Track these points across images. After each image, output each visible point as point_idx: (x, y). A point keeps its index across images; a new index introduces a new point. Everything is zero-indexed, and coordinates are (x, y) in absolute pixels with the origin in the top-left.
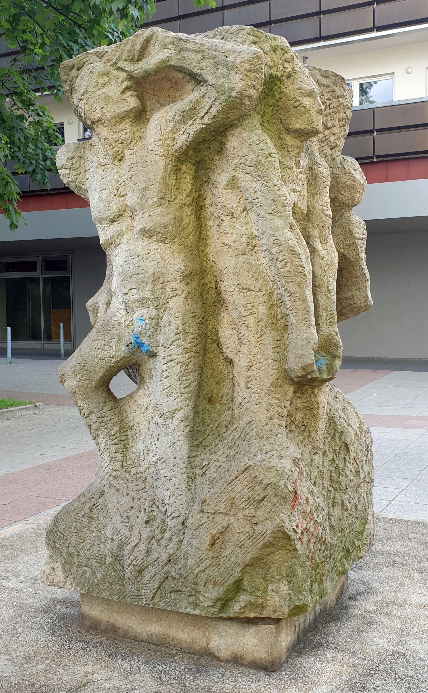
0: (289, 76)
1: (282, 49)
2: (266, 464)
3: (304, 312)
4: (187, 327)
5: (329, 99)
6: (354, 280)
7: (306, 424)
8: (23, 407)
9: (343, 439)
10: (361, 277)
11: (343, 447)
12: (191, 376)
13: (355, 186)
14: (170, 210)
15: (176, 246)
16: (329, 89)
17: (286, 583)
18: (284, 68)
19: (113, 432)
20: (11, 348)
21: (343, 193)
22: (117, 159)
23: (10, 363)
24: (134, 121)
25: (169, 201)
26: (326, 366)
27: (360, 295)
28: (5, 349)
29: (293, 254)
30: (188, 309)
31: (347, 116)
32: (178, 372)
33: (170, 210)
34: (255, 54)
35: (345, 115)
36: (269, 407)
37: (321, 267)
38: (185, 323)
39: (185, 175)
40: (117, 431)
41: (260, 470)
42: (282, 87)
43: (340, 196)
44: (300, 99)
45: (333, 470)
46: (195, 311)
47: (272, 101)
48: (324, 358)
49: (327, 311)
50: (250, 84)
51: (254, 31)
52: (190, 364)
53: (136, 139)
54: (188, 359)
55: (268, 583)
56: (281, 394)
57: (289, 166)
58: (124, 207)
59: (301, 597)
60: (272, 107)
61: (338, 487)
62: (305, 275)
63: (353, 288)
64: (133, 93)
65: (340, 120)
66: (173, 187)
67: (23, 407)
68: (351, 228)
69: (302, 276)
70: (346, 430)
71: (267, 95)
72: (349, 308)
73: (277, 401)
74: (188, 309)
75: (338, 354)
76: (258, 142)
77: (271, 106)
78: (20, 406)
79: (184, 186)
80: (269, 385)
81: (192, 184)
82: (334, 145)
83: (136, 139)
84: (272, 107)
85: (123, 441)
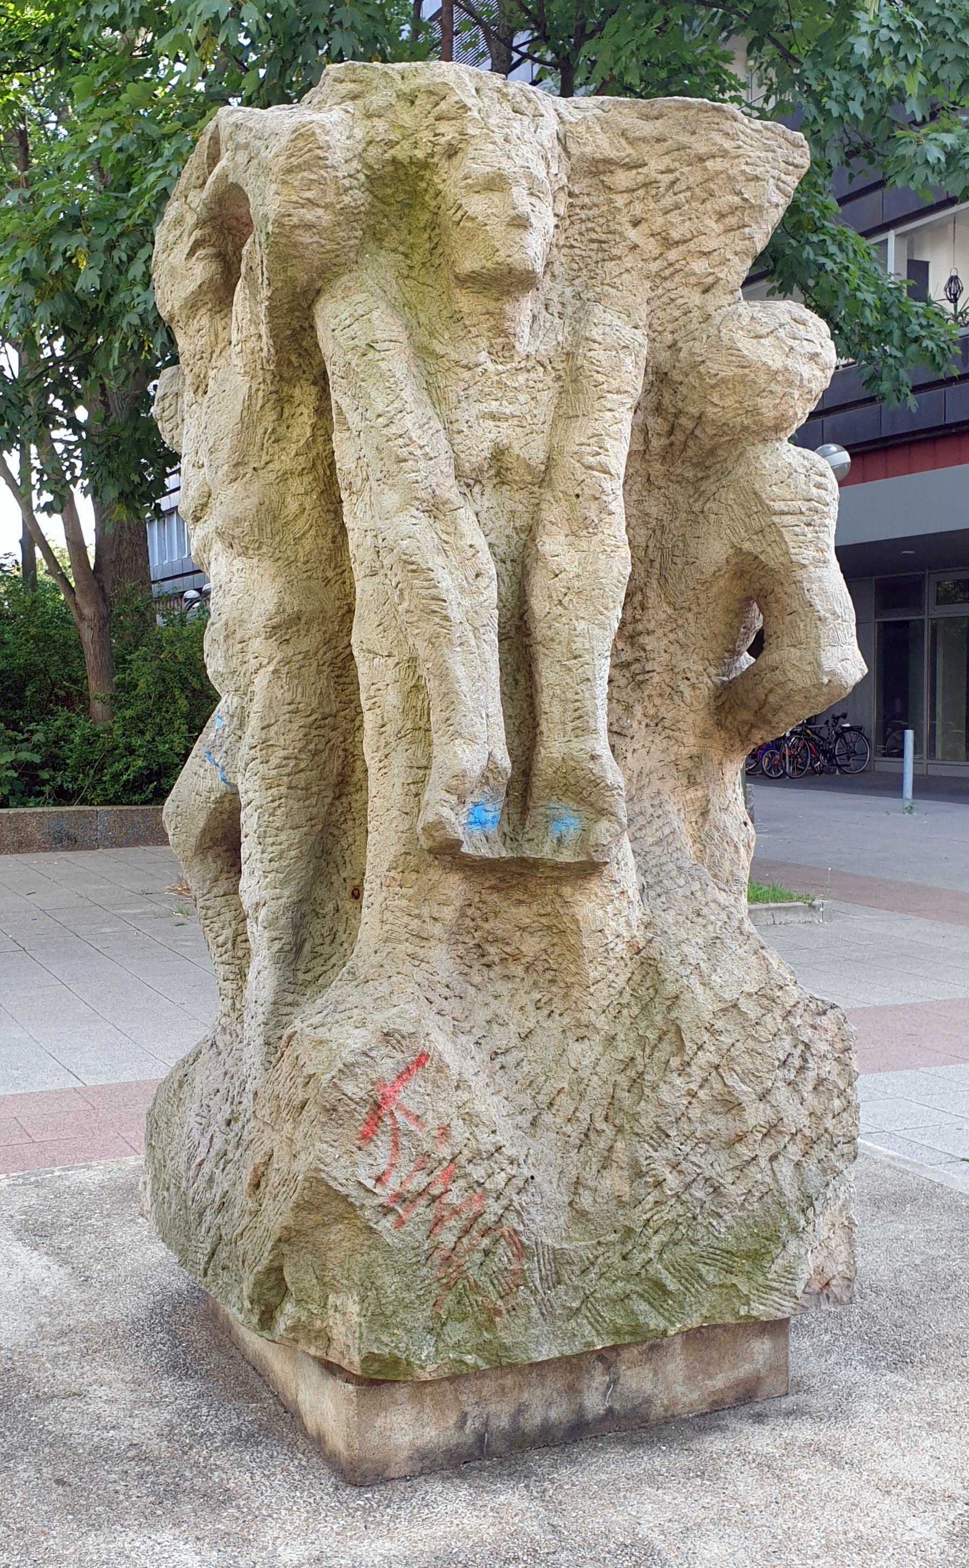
0: (452, 152)
1: (431, 93)
2: (322, 1033)
3: (445, 705)
4: (272, 734)
5: (669, 171)
6: (788, 618)
7: (555, 967)
8: (779, 905)
9: (674, 1015)
10: (800, 610)
11: (670, 1035)
12: (283, 837)
13: (749, 378)
14: (255, 487)
15: (267, 563)
16: (667, 144)
17: (357, 1299)
18: (436, 135)
19: (221, 940)
20: (914, 775)
21: (716, 400)
22: (200, 391)
23: (910, 810)
24: (218, 308)
25: (254, 469)
26: (579, 832)
27: (801, 658)
28: (900, 777)
29: (413, 571)
30: (279, 696)
31: (746, 200)
32: (255, 826)
33: (255, 487)
34: (295, 131)
35: (737, 199)
36: (388, 915)
37: (550, 597)
38: (269, 726)
39: (302, 409)
40: (227, 939)
41: (306, 1043)
42: (436, 181)
43: (710, 410)
44: (463, 201)
45: (626, 1085)
46: (299, 699)
47: (425, 217)
48: (576, 814)
49: (564, 701)
50: (294, 198)
51: (354, 70)
52: (278, 812)
53: (221, 346)
54: (273, 801)
55: (328, 1291)
56: (416, 888)
57: (465, 362)
58: (206, 489)
59: (385, 1338)
60: (429, 231)
61: (627, 1127)
62: (446, 618)
63: (786, 640)
64: (211, 251)
65: (721, 216)
66: (267, 437)
67: (779, 905)
68: (757, 486)
69: (437, 620)
70: (687, 996)
71: (410, 206)
72: (780, 691)
73: (405, 903)
74: (279, 696)
75: (606, 806)
76: (348, 322)
77: (425, 229)
78: (776, 901)
79: (295, 433)
80: (386, 866)
81: (314, 426)
82: (710, 279)
83: (221, 346)
84: (429, 231)
85: (239, 958)
